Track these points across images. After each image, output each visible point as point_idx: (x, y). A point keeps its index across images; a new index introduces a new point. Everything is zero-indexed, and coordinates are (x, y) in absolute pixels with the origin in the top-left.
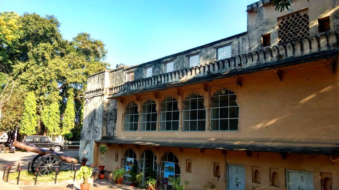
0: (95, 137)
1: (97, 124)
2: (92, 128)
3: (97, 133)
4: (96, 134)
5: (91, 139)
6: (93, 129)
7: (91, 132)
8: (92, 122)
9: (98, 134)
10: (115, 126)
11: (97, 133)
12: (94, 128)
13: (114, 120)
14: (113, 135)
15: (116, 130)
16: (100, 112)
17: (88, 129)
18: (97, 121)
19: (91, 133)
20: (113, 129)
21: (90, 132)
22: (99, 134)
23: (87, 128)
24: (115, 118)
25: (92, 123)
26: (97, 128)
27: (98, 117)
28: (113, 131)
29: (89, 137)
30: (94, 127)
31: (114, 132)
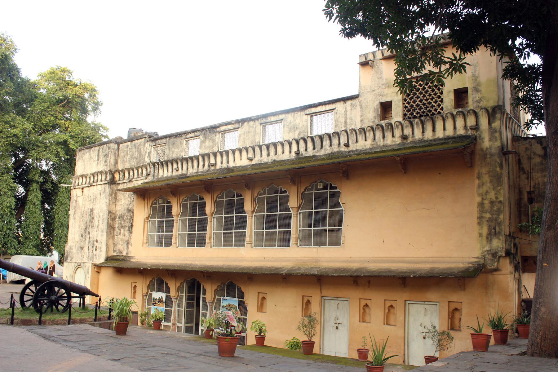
0: (93, 258)
1: (97, 234)
2: (87, 241)
4: (94, 252)
5: (86, 261)
6: (89, 243)
7: (84, 249)
8: (88, 230)
9: (98, 250)
10: (131, 238)
11: (96, 250)
12: (92, 242)
13: (127, 228)
14: (127, 253)
15: (131, 246)
16: (101, 214)
17: (79, 242)
18: (95, 230)
19: (86, 249)
20: (126, 243)
21: (82, 248)
22: (101, 251)
23: (77, 242)
24: (130, 225)
25: (87, 233)
26: (97, 241)
27: (99, 222)
28: (126, 247)
29: (80, 257)
30: (91, 239)
31: (128, 248)
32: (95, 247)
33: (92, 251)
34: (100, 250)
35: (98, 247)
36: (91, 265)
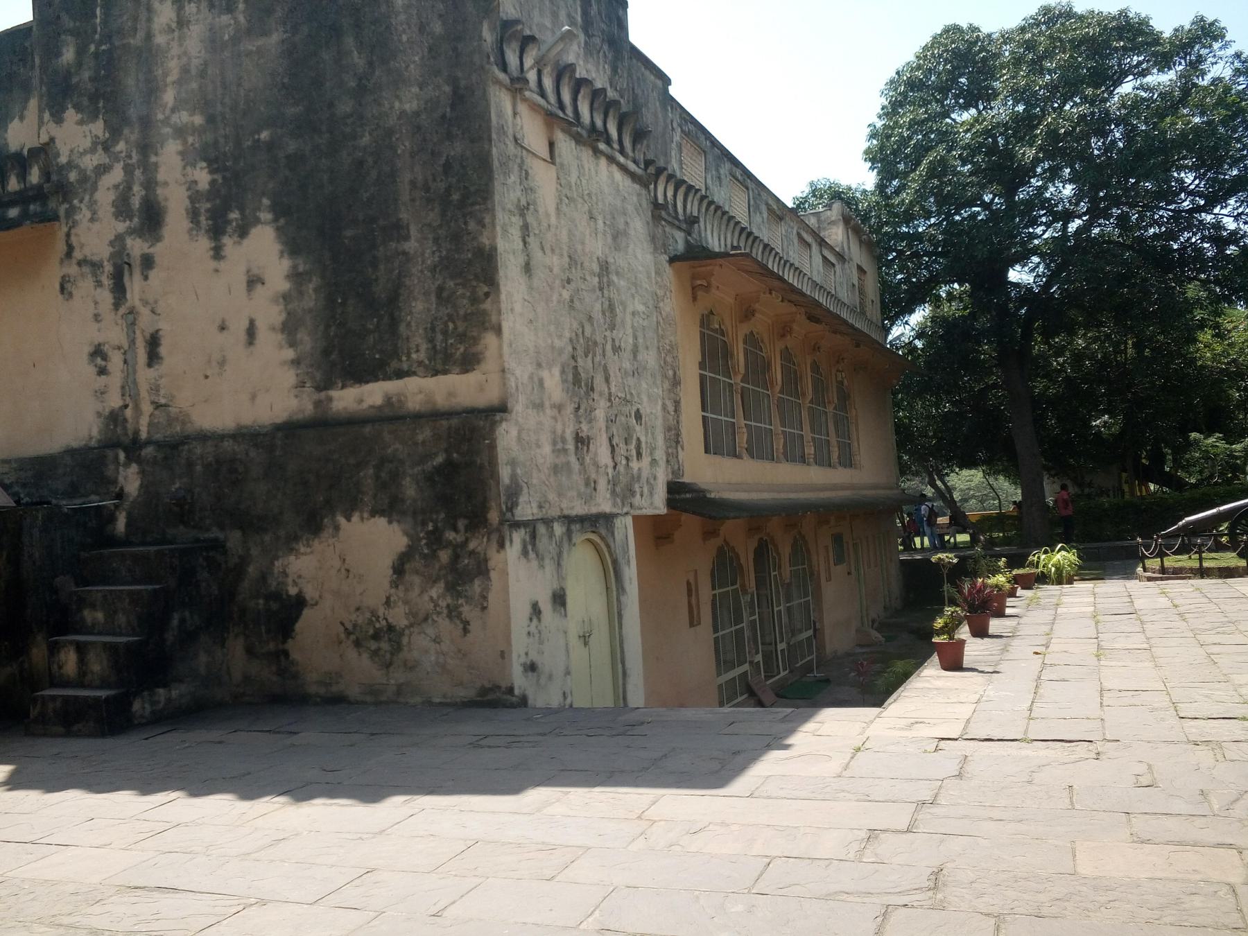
0: (633, 494)
3: (639, 455)
9: (646, 460)
11: (639, 455)
32: (634, 442)
33: (624, 462)
34: (649, 459)
35: (643, 445)
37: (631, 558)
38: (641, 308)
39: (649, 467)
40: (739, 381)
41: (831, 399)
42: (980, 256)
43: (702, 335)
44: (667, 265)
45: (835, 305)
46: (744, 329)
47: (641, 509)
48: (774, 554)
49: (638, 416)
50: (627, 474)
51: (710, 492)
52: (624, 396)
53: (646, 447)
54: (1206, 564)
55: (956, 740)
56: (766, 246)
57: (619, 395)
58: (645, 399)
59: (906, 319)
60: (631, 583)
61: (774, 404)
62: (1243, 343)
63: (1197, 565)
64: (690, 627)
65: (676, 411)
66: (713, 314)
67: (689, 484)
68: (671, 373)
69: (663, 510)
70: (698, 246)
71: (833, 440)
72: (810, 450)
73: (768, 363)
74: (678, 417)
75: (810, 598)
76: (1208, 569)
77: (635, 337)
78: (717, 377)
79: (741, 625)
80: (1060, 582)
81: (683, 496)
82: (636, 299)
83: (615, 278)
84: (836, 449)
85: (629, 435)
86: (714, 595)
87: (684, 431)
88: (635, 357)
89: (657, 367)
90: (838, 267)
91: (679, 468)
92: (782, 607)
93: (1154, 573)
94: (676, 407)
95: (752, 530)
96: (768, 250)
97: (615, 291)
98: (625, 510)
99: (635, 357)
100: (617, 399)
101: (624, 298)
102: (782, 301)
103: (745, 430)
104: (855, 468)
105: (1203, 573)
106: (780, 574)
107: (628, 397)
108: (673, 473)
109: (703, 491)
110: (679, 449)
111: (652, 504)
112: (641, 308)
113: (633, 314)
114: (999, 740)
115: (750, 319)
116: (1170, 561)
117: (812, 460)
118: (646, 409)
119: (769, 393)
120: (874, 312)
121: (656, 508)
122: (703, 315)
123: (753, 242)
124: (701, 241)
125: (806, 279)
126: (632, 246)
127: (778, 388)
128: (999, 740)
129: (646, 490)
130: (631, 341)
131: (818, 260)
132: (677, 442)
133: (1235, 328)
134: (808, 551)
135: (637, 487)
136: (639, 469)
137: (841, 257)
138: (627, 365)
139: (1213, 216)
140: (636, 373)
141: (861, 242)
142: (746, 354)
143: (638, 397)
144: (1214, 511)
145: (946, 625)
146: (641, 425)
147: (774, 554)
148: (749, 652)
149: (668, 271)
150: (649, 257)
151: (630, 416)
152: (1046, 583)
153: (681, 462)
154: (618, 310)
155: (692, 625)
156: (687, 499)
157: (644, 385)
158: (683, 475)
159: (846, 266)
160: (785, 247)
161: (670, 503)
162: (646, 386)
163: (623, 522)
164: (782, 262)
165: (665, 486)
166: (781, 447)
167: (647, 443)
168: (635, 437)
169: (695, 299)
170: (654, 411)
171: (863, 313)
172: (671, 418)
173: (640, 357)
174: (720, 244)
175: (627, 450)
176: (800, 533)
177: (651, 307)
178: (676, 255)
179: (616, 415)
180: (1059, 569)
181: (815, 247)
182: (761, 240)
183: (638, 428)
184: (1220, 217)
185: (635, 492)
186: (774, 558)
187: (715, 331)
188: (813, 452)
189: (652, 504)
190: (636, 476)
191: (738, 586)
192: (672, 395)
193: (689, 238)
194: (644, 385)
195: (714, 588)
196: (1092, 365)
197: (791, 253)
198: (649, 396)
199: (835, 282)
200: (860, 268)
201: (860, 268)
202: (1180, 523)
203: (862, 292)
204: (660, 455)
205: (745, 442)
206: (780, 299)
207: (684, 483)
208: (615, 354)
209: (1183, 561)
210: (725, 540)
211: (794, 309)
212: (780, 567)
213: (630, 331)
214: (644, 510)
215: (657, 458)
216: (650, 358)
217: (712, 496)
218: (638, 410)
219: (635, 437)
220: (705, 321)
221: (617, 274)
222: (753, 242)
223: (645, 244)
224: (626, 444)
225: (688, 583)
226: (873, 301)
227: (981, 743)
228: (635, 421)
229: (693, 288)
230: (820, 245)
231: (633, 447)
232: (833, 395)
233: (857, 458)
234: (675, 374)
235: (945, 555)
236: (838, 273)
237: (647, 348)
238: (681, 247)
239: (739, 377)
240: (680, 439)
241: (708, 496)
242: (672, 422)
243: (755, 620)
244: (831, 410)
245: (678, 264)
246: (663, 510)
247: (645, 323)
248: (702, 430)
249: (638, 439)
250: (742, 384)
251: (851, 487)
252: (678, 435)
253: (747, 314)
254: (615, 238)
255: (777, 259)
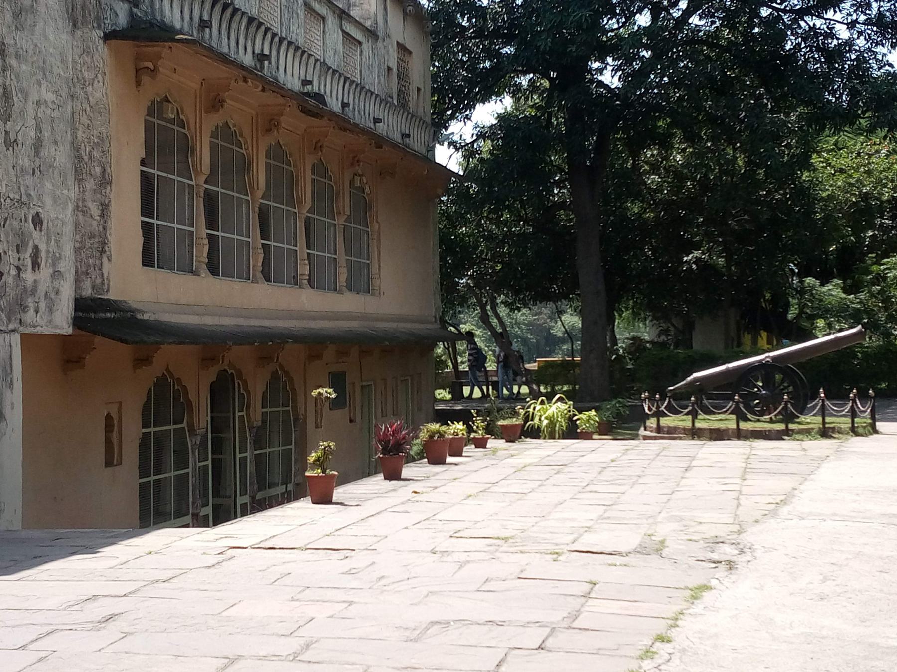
0: (24, 308)
3: (36, 265)
9: (45, 272)
11: (36, 265)
32: (30, 251)
33: (14, 272)
34: (51, 271)
35: (43, 254)
36: (16, 339)
37: (15, 381)
38: (50, 96)
39: (49, 280)
40: (202, 182)
41: (341, 209)
42: (542, 47)
43: (149, 129)
44: (101, 42)
45: (357, 94)
46: (214, 120)
47: (35, 326)
48: (242, 391)
49: (38, 221)
50: (18, 286)
51: (143, 312)
52: (17, 197)
53: (47, 257)
54: (698, 425)
55: (246, 548)
56: (251, 20)
57: (12, 196)
58: (48, 201)
59: (468, 113)
60: (13, 408)
61: (254, 212)
62: (881, 172)
63: (688, 424)
64: (106, 467)
65: (102, 215)
66: (168, 101)
67: (115, 301)
68: (98, 170)
69: (67, 330)
70: (145, 22)
71: (342, 258)
72: (304, 269)
73: (249, 162)
74: (105, 222)
75: (292, 446)
76: (700, 429)
77: (39, 129)
78: (170, 176)
79: (186, 471)
80: (552, 437)
81: (102, 315)
82: (44, 87)
83: (14, 62)
84: (344, 270)
85: (22, 242)
86: (146, 436)
87: (112, 238)
88: (37, 153)
89: (69, 166)
90: (367, 46)
91: (103, 284)
92: (248, 455)
93: (651, 431)
94: (103, 210)
95: (207, 360)
96: (255, 24)
97: (13, 77)
98: (11, 326)
99: (37, 153)
100: (8, 200)
101: (25, 85)
102: (263, 90)
103: (206, 242)
104: (373, 294)
105: (694, 433)
106: (248, 415)
107: (24, 198)
108: (93, 287)
109: (133, 311)
110: (105, 260)
111: (50, 321)
112: (50, 96)
113: (38, 103)
114: (280, 548)
115: (218, 110)
116: (668, 421)
117: (306, 282)
118: (49, 212)
119: (249, 198)
120: (423, 105)
121: (56, 327)
122: (153, 102)
123: (233, 15)
124: (153, 13)
125: (312, 60)
126: (40, 25)
127: (260, 193)
128: (280, 548)
129: (43, 305)
130: (33, 134)
131: (335, 37)
132: (103, 252)
133: (877, 152)
134: (293, 390)
135: (30, 302)
136: (35, 281)
137: (372, 34)
138: (25, 162)
139: (823, 21)
140: (37, 171)
141: (405, 14)
142: (213, 148)
143: (39, 199)
144: (722, 368)
145: (318, 459)
146: (41, 231)
147: (242, 391)
148: (193, 503)
149: (102, 51)
150: (65, 37)
151: (26, 221)
152: (538, 437)
153: (105, 276)
154: (15, 99)
155: (109, 463)
156: (106, 319)
157: (49, 185)
158: (108, 291)
159: (380, 44)
160: (285, 22)
161: (77, 322)
162: (51, 187)
163: (7, 340)
164: (276, 39)
165: (72, 305)
166: (260, 264)
167: (48, 252)
168: (31, 244)
169: (138, 83)
170: (61, 216)
171: (403, 105)
172: (95, 223)
173: (44, 153)
174: (182, 19)
175: (19, 259)
176: (281, 367)
177: (63, 95)
178: (114, 31)
179: (6, 219)
180: (552, 422)
181: (332, 22)
182: (243, 13)
183: (36, 234)
184: (832, 22)
185: (27, 306)
186: (241, 396)
187: (172, 121)
188: (307, 272)
189: (50, 321)
190: (29, 290)
191: (184, 425)
192: (99, 196)
193: (134, 10)
194: (49, 185)
195: (145, 424)
196: (694, 186)
197: (294, 28)
198: (55, 200)
199: (361, 65)
200: (401, 47)
201: (401, 47)
202: (689, 379)
203: (403, 76)
204: (67, 266)
205: (205, 255)
206: (260, 88)
207: (109, 300)
208: (8, 149)
209: (681, 421)
210: (167, 369)
211: (281, 100)
212: (248, 407)
213: (31, 123)
214: (38, 328)
215: (62, 270)
216: (61, 156)
217: (146, 317)
218: (37, 213)
219: (31, 244)
220: (155, 109)
221: (18, 56)
222: (233, 15)
223: (60, 23)
224: (18, 252)
225: (109, 417)
226: (419, 89)
227: (265, 550)
228: (32, 226)
229: (137, 71)
230: (341, 18)
231: (27, 255)
232: (345, 204)
233: (376, 282)
234: (104, 171)
235: (325, 389)
236: (365, 53)
237: (56, 143)
238: (122, 20)
239: (204, 178)
240: (106, 249)
241: (139, 316)
242: (95, 226)
243: (207, 466)
244: (342, 221)
245: (113, 42)
246: (67, 330)
247: (56, 114)
248: (140, 240)
249: (36, 247)
250: (206, 186)
251: (363, 317)
252: (104, 243)
253: (215, 104)
254: (17, 15)
255: (269, 36)
